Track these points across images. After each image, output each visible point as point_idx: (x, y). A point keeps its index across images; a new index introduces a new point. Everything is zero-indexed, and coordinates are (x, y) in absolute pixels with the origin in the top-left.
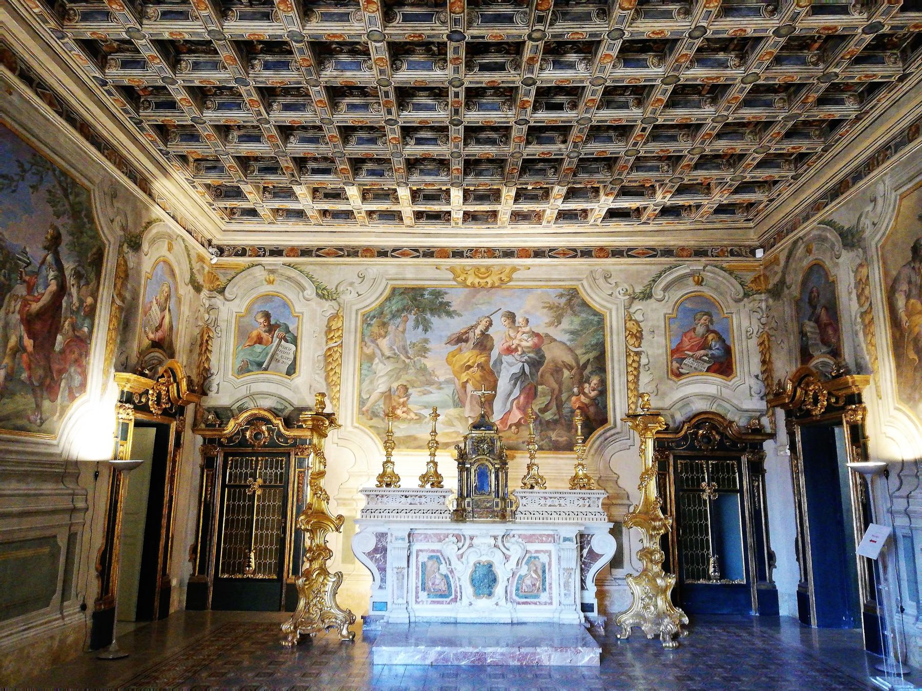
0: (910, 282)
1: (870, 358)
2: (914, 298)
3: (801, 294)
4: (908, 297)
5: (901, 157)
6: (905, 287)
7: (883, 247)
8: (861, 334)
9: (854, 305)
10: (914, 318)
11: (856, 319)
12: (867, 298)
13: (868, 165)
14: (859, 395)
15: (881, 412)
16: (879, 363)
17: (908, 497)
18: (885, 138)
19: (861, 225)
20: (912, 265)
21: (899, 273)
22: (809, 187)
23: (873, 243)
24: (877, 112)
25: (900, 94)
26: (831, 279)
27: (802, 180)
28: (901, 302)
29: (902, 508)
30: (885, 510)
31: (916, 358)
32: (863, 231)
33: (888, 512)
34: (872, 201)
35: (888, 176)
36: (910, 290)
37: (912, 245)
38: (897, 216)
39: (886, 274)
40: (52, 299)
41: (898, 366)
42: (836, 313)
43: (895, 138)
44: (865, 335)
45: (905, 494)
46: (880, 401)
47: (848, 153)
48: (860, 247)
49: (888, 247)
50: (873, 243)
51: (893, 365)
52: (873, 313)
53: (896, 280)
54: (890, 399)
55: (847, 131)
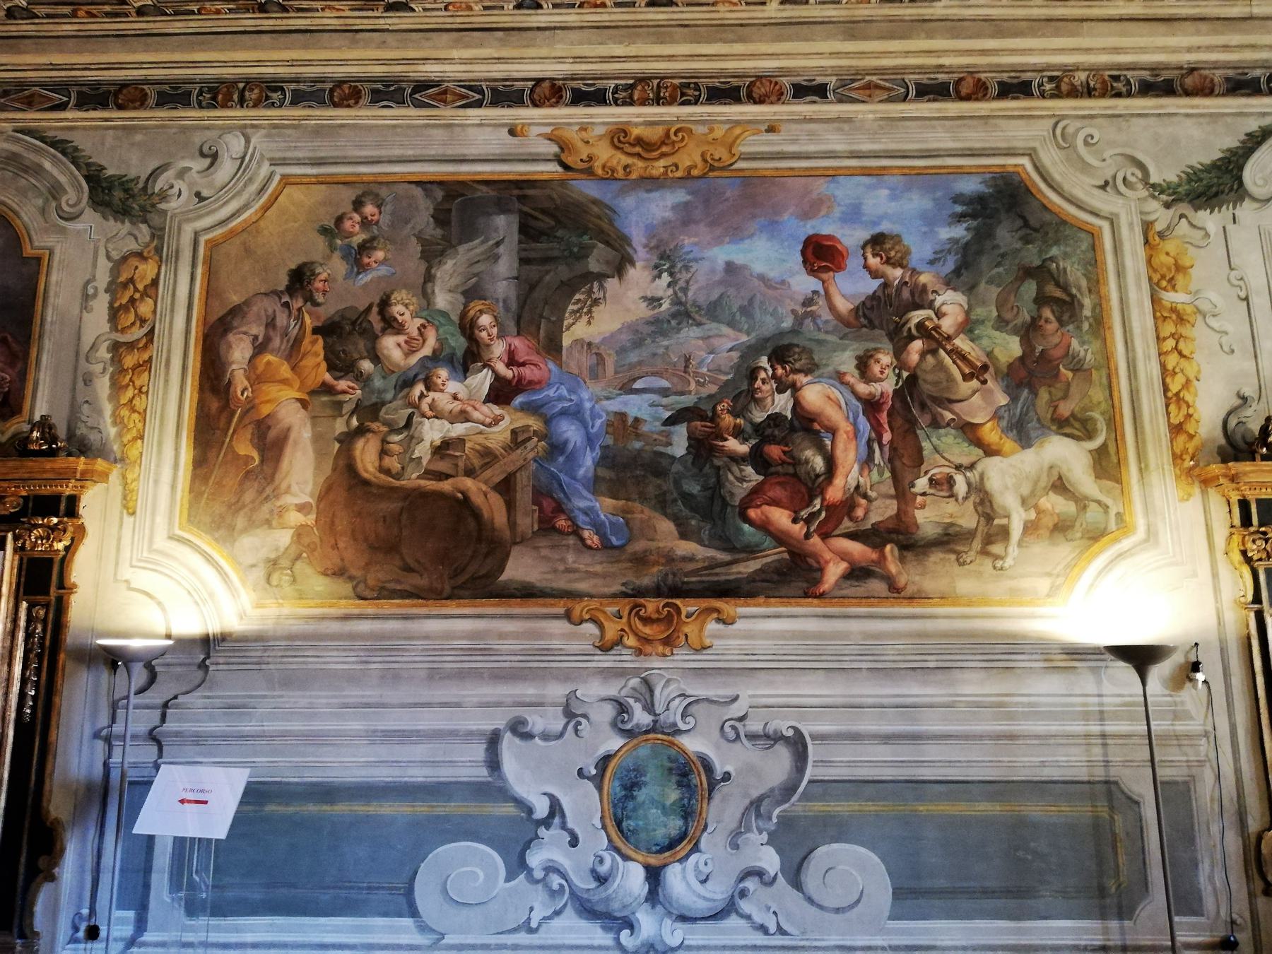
0: (271, 324)
1: (120, 435)
2: (274, 352)
3: (896, 490)
4: (260, 348)
5: (307, 118)
6: (257, 330)
7: (213, 246)
8: (103, 385)
9: (97, 322)
10: (265, 387)
11: (94, 347)
12: (143, 321)
13: (214, 92)
14: (73, 501)
15: (126, 540)
16: (147, 449)
17: (166, 705)
18: (280, 70)
19: (160, 184)
20: (286, 298)
21: (247, 303)
22: (37, 51)
23: (188, 230)
24: (308, 22)
25: (367, 24)
26: (28, 251)
27: (26, 27)
28: (239, 352)
29: (143, 728)
30: (88, 731)
31: (255, 455)
32: (163, 196)
33: (96, 735)
34: (203, 155)
35: (263, 132)
36: (268, 339)
37: (293, 267)
38: (266, 208)
39: (210, 292)
40: (218, 353)
41: (201, 463)
42: (30, 321)
43: (297, 81)
44: (117, 387)
45: (160, 701)
46: (128, 520)
47: (191, 48)
48: (145, 221)
49: (233, 248)
50: (188, 230)
51: (186, 455)
52: (154, 350)
53: (237, 312)
54: (161, 520)
55: (218, 12)
